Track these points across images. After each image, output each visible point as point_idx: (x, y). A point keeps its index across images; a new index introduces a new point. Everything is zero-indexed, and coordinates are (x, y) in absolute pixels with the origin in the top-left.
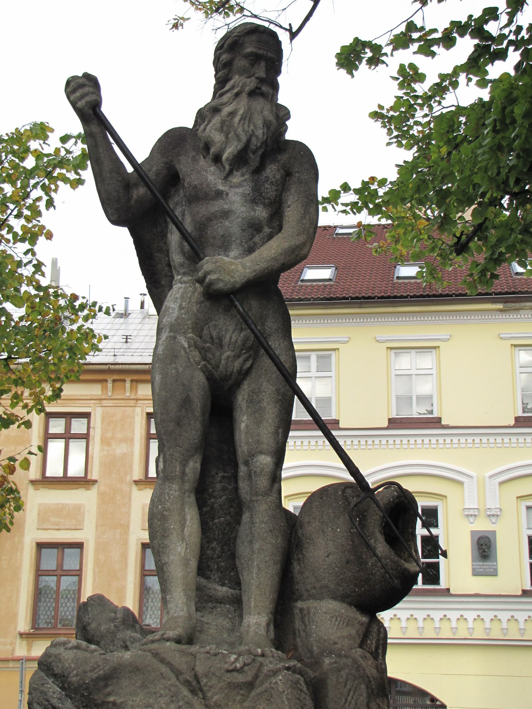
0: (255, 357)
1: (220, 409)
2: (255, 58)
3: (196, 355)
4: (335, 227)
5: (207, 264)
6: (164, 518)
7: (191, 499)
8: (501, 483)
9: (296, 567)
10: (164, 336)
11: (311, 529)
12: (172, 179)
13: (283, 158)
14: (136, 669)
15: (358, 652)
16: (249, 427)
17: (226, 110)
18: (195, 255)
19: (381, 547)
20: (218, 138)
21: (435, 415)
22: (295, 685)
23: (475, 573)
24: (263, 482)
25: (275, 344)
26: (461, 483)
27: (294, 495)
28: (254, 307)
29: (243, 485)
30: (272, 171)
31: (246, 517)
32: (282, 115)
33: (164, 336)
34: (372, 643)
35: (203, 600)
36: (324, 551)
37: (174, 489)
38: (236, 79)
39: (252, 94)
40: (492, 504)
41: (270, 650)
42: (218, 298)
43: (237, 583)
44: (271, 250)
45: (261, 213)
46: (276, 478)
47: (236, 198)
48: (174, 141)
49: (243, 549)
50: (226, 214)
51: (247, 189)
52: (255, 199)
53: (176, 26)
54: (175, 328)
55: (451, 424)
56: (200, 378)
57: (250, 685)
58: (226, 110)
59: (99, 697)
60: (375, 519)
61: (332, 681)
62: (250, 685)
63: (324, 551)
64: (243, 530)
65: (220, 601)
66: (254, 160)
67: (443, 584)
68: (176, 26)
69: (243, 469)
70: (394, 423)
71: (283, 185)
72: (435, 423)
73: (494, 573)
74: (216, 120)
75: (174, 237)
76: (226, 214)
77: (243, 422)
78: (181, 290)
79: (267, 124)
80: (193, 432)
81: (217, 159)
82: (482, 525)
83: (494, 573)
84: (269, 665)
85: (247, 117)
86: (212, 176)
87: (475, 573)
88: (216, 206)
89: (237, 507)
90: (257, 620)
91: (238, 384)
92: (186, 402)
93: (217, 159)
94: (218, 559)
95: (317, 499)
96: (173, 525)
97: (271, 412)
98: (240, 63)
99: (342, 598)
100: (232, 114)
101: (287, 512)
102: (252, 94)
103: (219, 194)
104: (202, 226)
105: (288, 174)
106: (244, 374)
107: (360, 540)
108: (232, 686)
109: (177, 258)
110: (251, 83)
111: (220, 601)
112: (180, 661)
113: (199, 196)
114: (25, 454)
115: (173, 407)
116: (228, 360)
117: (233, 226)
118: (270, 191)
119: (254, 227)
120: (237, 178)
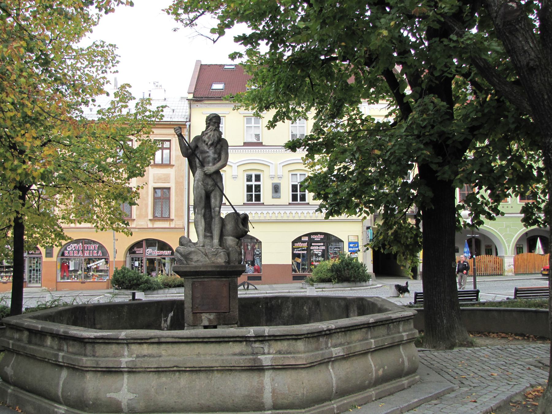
0: (215, 187)
1: (208, 197)
2: (215, 123)
3: (202, 186)
4: (224, 65)
5: (205, 169)
6: (197, 222)
7: (203, 218)
8: (283, 166)
9: (224, 230)
10: (196, 182)
11: (227, 222)
12: (197, 147)
13: (221, 143)
14: (194, 252)
15: (236, 247)
16: (214, 202)
17: (209, 134)
18: (202, 165)
19: (241, 226)
20: (207, 140)
21: (260, 141)
22: (225, 254)
23: (273, 198)
24: (217, 213)
25: (219, 184)
26: (269, 166)
27: (223, 216)
28: (215, 176)
29: (213, 214)
30: (219, 146)
31: (213, 220)
32: (221, 133)
33: (196, 182)
34: (239, 245)
35: (205, 237)
36: (229, 227)
37: (199, 216)
38: (211, 127)
39: (214, 130)
40: (280, 173)
41: (219, 247)
42: (207, 176)
43: (211, 233)
44: (219, 164)
45: (216, 156)
46: (219, 212)
47: (211, 153)
48: (197, 139)
49: (213, 227)
50: (209, 156)
51: (213, 151)
52: (215, 153)
53: (175, 30)
54: (198, 181)
55: (266, 145)
56: (203, 192)
57: (216, 254)
58: (209, 134)
59: (188, 257)
60: (240, 221)
61: (231, 252)
62: (216, 254)
63: (229, 227)
64: (213, 223)
65: (208, 236)
66: (215, 144)
67: (262, 201)
68: (175, 30)
69: (213, 210)
70: (246, 144)
71: (221, 150)
72: (261, 144)
73: (280, 198)
74: (207, 136)
75: (197, 161)
76: (209, 156)
77: (213, 201)
78: (198, 172)
79: (218, 137)
80: (203, 204)
81: (207, 144)
82: (276, 181)
83: (280, 198)
84: (220, 251)
85: (214, 136)
86: (206, 148)
87: (273, 198)
88: (207, 155)
89: (211, 218)
90: (216, 241)
91: (211, 192)
92: (201, 197)
93: (207, 144)
94: (208, 228)
95: (228, 215)
96: (199, 224)
97: (218, 199)
98: (212, 123)
99: (233, 236)
100: (210, 135)
101: (221, 218)
102: (214, 130)
103: (207, 152)
104: (204, 159)
105: (222, 146)
106: (213, 190)
107: (237, 224)
108: (213, 255)
109: (198, 165)
110: (214, 128)
111: (208, 236)
112: (203, 250)
113: (204, 152)
114: (142, 185)
115: (199, 199)
116: (209, 187)
117: (210, 159)
118: (218, 151)
119: (215, 159)
120: (211, 148)
